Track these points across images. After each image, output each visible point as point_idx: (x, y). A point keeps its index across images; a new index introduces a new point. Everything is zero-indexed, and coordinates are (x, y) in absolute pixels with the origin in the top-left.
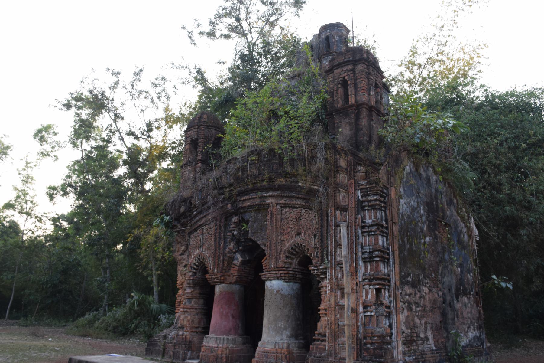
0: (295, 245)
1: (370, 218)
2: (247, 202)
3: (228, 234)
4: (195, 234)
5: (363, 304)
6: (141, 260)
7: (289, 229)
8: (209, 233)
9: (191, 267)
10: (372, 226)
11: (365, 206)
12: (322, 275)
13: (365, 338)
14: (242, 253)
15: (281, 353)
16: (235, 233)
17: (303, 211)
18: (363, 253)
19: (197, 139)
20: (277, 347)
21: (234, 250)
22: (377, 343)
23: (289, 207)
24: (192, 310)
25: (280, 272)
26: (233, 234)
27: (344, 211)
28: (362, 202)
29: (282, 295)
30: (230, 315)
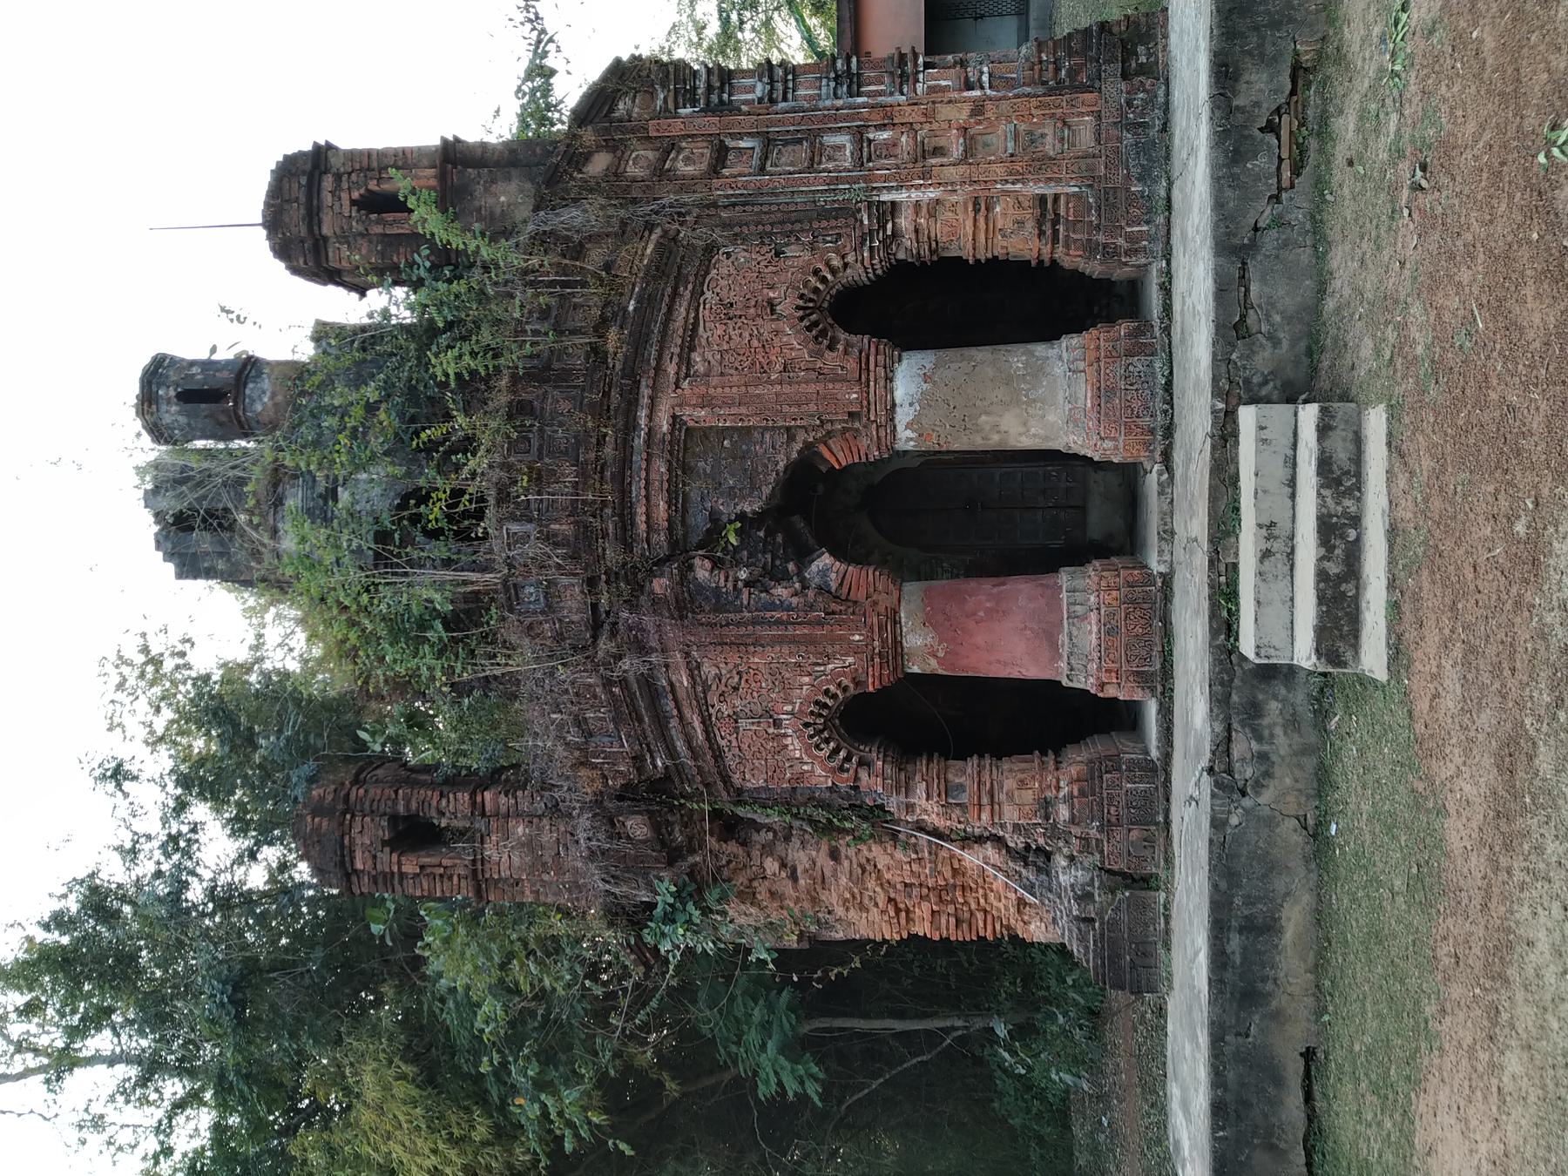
0: (801, 319)
1: (752, 89)
3: (745, 596)
4: (730, 761)
5: (961, 90)
6: (803, 1098)
7: (755, 343)
8: (736, 689)
9: (841, 769)
10: (772, 82)
12: (885, 230)
13: (1044, 83)
14: (804, 556)
17: (708, 294)
18: (836, 96)
19: (394, 819)
20: (1081, 365)
21: (797, 585)
23: (692, 349)
24: (986, 777)
26: (747, 584)
28: (708, 103)
30: (995, 590)
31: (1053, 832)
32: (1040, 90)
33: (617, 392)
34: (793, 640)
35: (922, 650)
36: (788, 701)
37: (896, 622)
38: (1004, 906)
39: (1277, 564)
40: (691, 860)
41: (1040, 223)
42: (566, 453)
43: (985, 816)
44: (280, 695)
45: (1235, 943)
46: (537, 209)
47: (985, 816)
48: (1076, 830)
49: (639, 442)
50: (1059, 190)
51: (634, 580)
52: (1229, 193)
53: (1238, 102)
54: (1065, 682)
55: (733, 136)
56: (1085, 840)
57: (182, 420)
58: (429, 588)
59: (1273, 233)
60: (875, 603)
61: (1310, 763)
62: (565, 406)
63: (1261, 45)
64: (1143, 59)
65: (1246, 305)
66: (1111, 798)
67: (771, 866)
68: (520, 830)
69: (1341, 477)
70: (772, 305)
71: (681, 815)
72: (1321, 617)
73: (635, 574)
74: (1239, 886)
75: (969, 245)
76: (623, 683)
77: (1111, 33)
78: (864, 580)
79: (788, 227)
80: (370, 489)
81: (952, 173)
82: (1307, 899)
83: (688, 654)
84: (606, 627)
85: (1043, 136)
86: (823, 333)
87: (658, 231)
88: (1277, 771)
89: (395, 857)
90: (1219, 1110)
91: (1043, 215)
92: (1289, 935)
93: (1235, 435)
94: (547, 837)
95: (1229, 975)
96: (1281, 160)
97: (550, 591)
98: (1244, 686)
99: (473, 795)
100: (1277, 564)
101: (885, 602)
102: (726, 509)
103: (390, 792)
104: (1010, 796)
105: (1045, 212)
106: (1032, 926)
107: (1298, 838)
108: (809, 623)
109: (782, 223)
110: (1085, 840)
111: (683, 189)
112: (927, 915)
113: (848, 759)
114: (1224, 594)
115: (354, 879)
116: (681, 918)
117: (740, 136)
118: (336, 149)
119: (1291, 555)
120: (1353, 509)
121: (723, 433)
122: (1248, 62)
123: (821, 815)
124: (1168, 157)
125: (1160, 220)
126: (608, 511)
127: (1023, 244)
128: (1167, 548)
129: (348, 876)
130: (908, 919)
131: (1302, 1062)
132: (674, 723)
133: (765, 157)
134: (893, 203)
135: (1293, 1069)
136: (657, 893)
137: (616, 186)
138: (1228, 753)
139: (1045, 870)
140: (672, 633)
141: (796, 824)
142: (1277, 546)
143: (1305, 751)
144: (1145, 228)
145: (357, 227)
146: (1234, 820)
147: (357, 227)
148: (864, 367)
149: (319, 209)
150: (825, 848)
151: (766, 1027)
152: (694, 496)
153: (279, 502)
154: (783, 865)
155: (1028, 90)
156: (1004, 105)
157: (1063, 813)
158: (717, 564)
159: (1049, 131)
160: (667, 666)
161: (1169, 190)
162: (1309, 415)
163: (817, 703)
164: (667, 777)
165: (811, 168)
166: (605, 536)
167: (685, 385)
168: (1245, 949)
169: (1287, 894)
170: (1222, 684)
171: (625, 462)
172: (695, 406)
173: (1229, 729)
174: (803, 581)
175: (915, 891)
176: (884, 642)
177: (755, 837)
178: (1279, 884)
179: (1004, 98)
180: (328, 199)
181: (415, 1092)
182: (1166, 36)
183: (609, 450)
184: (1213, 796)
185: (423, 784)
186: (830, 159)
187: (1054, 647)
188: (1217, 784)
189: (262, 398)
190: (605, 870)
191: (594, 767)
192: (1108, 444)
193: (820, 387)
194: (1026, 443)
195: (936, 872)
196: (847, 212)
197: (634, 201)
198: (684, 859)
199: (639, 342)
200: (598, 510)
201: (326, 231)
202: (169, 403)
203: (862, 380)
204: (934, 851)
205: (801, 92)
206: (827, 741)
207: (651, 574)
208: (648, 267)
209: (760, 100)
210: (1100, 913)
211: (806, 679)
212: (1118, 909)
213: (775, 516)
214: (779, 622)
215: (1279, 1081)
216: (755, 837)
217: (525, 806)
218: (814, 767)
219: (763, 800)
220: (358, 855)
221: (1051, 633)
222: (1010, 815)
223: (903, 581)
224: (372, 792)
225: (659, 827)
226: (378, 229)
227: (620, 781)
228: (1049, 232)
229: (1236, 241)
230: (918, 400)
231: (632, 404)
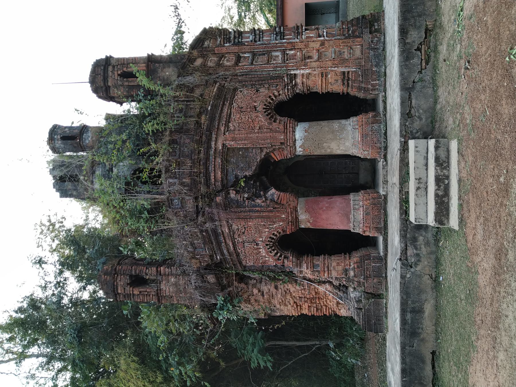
0: (265, 112)
1: (249, 37)
2: (216, 175)
3: (247, 203)
5: (317, 38)
7: (250, 120)
8: (244, 233)
9: (278, 259)
11: (239, 42)
12: (292, 83)
13: (344, 35)
14: (266, 189)
16: (246, 196)
17: (234, 104)
18: (276, 40)
19: (131, 276)
20: (357, 127)
21: (264, 199)
23: (229, 122)
24: (326, 262)
26: (247, 199)
27: (240, 60)
28: (234, 42)
31: (348, 280)
32: (343, 37)
33: (205, 136)
34: (262, 217)
35: (305, 220)
37: (296, 211)
38: (332, 304)
39: (422, 192)
40: (229, 289)
41: (343, 81)
43: (326, 275)
44: (94, 236)
45: (409, 316)
46: (178, 77)
47: (326, 275)
49: (212, 152)
50: (349, 70)
51: (210, 197)
52: (405, 70)
54: (352, 231)
55: (242, 53)
56: (359, 282)
57: (62, 146)
58: (143, 200)
59: (420, 84)
60: (289, 205)
61: (433, 257)
62: (187, 141)
63: (415, 23)
64: (376, 27)
65: (411, 107)
66: (367, 269)
67: (255, 291)
69: (442, 163)
70: (255, 107)
71: (225, 274)
72: (436, 209)
73: (211, 195)
75: (320, 88)
76: (207, 231)
78: (286, 197)
79: (261, 82)
80: (123, 168)
81: (314, 64)
82: (432, 302)
83: (228, 222)
84: (201, 213)
85: (344, 52)
86: (272, 117)
87: (218, 84)
88: (422, 259)
90: (404, 371)
91: (344, 78)
92: (426, 314)
93: (408, 149)
94: (181, 282)
95: (407, 327)
96: (422, 60)
97: (182, 201)
98: (411, 232)
99: (157, 268)
100: (422, 192)
101: (293, 204)
102: (240, 174)
106: (342, 311)
107: (429, 282)
108: (268, 211)
109: (259, 81)
110: (359, 282)
112: (307, 307)
113: (281, 256)
114: (404, 202)
115: (118, 296)
116: (226, 308)
117: (245, 53)
118: (113, 58)
119: (426, 188)
120: (447, 174)
121: (239, 149)
122: (411, 28)
123: (272, 274)
124: (385, 59)
125: (383, 79)
126: (202, 175)
127: (338, 88)
128: (385, 186)
129: (116, 295)
130: (301, 309)
132: (223, 244)
133: (253, 60)
134: (295, 74)
137: (204, 69)
138: (406, 253)
140: (223, 215)
141: (264, 277)
142: (422, 186)
143: (431, 253)
145: (120, 83)
146: (408, 276)
147: (120, 83)
148: (285, 128)
149: (107, 77)
150: (273, 285)
151: (254, 344)
152: (230, 170)
153: (93, 173)
154: (259, 291)
155: (339, 37)
156: (331, 42)
157: (352, 273)
158: (237, 192)
159: (346, 50)
160: (221, 226)
161: (385, 70)
162: (432, 143)
163: (270, 238)
164: (221, 262)
165: (268, 63)
166: (201, 183)
167: (227, 134)
168: (412, 318)
169: (426, 300)
170: (404, 231)
171: (207, 159)
172: (230, 141)
173: (406, 246)
174: (266, 198)
175: (303, 300)
176: (292, 217)
177: (250, 282)
178: (423, 297)
180: (110, 74)
181: (138, 366)
182: (384, 20)
183: (202, 155)
184: (401, 268)
185: (141, 265)
186: (274, 60)
187: (349, 219)
188: (402, 264)
189: (88, 139)
190: (201, 293)
191: (197, 259)
192: (366, 152)
193: (271, 134)
194: (339, 152)
195: (310, 293)
196: (280, 77)
197: (210, 74)
198: (227, 289)
199: (212, 120)
201: (110, 84)
203: (285, 132)
204: (309, 286)
205: (265, 38)
206: (274, 250)
207: (216, 196)
208: (215, 95)
209: (251, 41)
210: (364, 306)
211: (267, 230)
213: (256, 177)
214: (258, 211)
215: (423, 362)
216: (250, 282)
217: (174, 272)
219: (252, 269)
220: (119, 288)
221: (347, 214)
222: (334, 274)
223: (299, 197)
224: (124, 267)
226: (126, 84)
228: (346, 84)
230: (303, 138)
231: (209, 140)
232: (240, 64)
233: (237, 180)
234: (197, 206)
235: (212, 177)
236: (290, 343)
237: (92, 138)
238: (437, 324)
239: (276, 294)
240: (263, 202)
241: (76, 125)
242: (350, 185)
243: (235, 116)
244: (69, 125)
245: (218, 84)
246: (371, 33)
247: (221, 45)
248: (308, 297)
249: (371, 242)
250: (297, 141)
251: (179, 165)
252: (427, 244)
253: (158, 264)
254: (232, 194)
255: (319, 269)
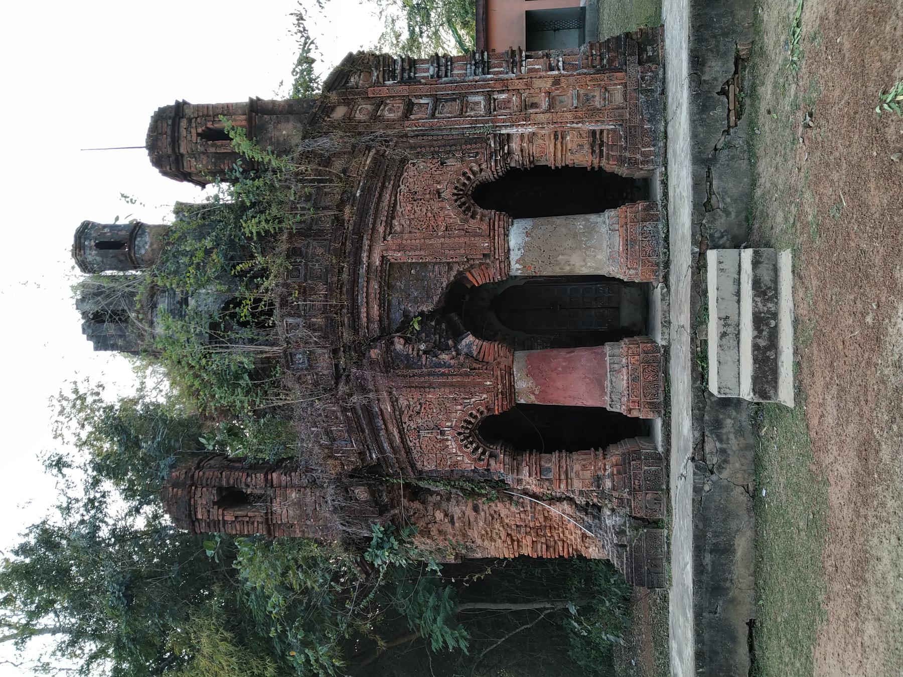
0: (456, 201)
1: (427, 70)
2: (370, 311)
3: (424, 359)
4: (415, 455)
5: (547, 71)
6: (458, 650)
7: (429, 214)
8: (418, 413)
9: (480, 459)
10: (439, 66)
11: (410, 77)
13: (594, 67)
14: (458, 336)
15: (626, 217)
16: (423, 347)
17: (402, 187)
18: (475, 74)
19: (220, 489)
20: (617, 227)
21: (454, 353)
22: (600, 49)
23: (393, 218)
25: (496, 228)
26: (425, 352)
28: (402, 78)
29: (533, 228)
30: (568, 356)
31: (602, 495)
32: (592, 71)
33: (350, 242)
34: (451, 385)
35: (526, 390)
36: (448, 420)
37: (511, 374)
38: (574, 538)
39: (730, 341)
40: (392, 512)
41: (592, 146)
42: (320, 278)
44: (154, 417)
45: (708, 559)
46: (304, 138)
48: (615, 494)
49: (363, 271)
50: (603, 127)
51: (359, 350)
52: (700, 129)
53: (705, 77)
54: (609, 408)
55: (416, 97)
56: (621, 499)
57: (99, 259)
58: (241, 355)
59: (726, 152)
60: (499, 363)
61: (750, 454)
62: (320, 251)
63: (717, 46)
64: (650, 54)
65: (711, 193)
66: (635, 475)
67: (439, 515)
68: (293, 495)
69: (766, 291)
70: (439, 192)
71: (387, 486)
73: (360, 346)
74: (710, 526)
75: (552, 159)
77: (632, 39)
78: (493, 350)
79: (448, 148)
80: (207, 298)
81: (542, 118)
82: (749, 533)
83: (390, 393)
84: (343, 377)
85: (594, 97)
86: (468, 209)
87: (374, 151)
88: (731, 459)
89: (220, 511)
91: (594, 141)
92: (739, 554)
94: (309, 499)
95: (704, 578)
96: (729, 110)
97: (311, 358)
98: (712, 411)
99: (266, 475)
100: (730, 341)
101: (504, 362)
102: (412, 309)
103: (217, 474)
104: (577, 475)
105: (595, 140)
107: (744, 498)
108: (461, 375)
109: (445, 146)
110: (621, 499)
111: (387, 127)
112: (530, 543)
113: (483, 453)
114: (700, 358)
115: (197, 524)
116: (387, 546)
117: (421, 97)
118: (189, 104)
119: (738, 335)
123: (468, 486)
124: (665, 109)
125: (661, 144)
126: (345, 311)
127: (583, 158)
128: (666, 331)
129: (193, 522)
130: (519, 546)
131: (747, 628)
132: (382, 433)
133: (435, 109)
134: (508, 135)
135: (742, 632)
136: (373, 532)
138: (703, 448)
139: (598, 517)
140: (382, 381)
141: (454, 491)
142: (730, 330)
143: (747, 447)
144: (652, 149)
145: (200, 148)
146: (707, 488)
147: (200, 148)
148: (492, 228)
149: (179, 138)
150: (470, 505)
151: (436, 609)
152: (394, 302)
153: (154, 306)
154: (446, 515)
155: (585, 71)
156: (571, 79)
157: (608, 484)
158: (407, 341)
159: (597, 94)
160: (378, 400)
162: (747, 255)
163: (465, 421)
165: (461, 115)
166: (343, 325)
167: (389, 238)
168: (713, 562)
171: (354, 282)
173: (703, 435)
174: (457, 350)
175: (523, 530)
176: (504, 385)
177: (430, 499)
178: (733, 525)
179: (572, 75)
180: (184, 132)
181: (232, 648)
182: (663, 41)
183: (345, 276)
184: (695, 474)
185: (237, 469)
186: (472, 109)
187: (602, 388)
188: (697, 467)
189: (145, 246)
190: (343, 518)
191: (336, 458)
192: (632, 272)
193: (467, 239)
194: (585, 271)
196: (482, 140)
197: (360, 134)
198: (389, 511)
199: (363, 213)
200: (339, 310)
201: (182, 150)
202: (91, 249)
203: (491, 236)
204: (534, 506)
205: (456, 72)
206: (471, 443)
207: (370, 347)
209: (432, 76)
210: (630, 542)
211: (459, 407)
212: (640, 540)
213: (441, 313)
214: (443, 374)
215: (734, 639)
216: (430, 499)
217: (296, 481)
218: (463, 457)
221: (599, 380)
222: (577, 485)
224: (207, 473)
225: (374, 493)
226: (212, 150)
227: (351, 467)
229: (704, 156)
230: (523, 247)
231: (358, 249)
232: (412, 117)
233: (407, 319)
234: (337, 366)
235: (363, 315)
236: (501, 606)
237: (152, 244)
238: (757, 572)
239: (476, 521)
240: (453, 358)
241: (123, 222)
242: (604, 329)
243: (404, 208)
244: (111, 222)
245: (374, 151)
246: (640, 63)
247: (378, 84)
248: (532, 524)
249: (643, 429)
250: (511, 252)
251: (305, 292)
252: (740, 432)
253: (267, 468)
254: (399, 345)
255: (551, 476)
